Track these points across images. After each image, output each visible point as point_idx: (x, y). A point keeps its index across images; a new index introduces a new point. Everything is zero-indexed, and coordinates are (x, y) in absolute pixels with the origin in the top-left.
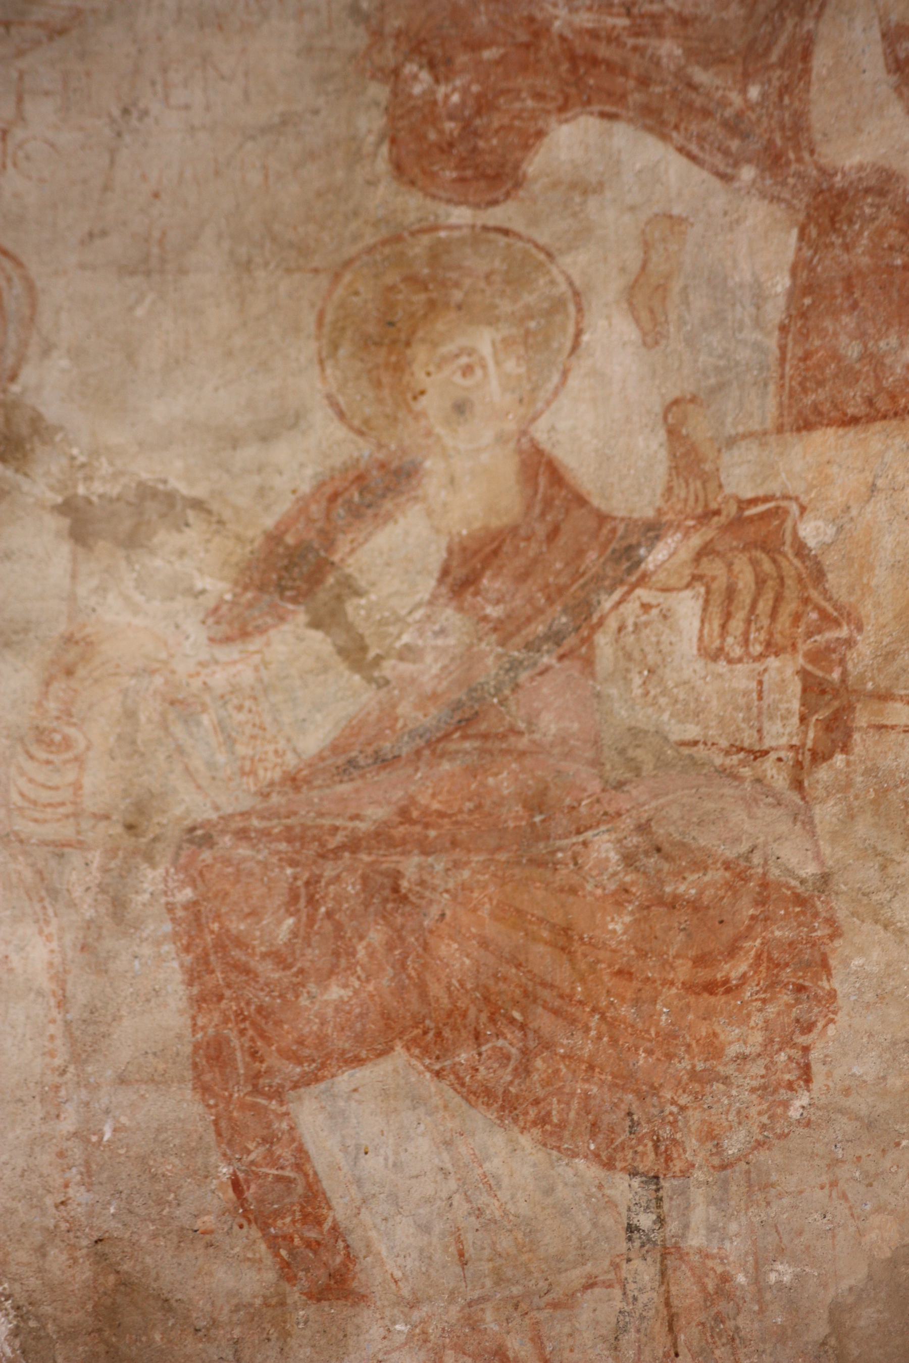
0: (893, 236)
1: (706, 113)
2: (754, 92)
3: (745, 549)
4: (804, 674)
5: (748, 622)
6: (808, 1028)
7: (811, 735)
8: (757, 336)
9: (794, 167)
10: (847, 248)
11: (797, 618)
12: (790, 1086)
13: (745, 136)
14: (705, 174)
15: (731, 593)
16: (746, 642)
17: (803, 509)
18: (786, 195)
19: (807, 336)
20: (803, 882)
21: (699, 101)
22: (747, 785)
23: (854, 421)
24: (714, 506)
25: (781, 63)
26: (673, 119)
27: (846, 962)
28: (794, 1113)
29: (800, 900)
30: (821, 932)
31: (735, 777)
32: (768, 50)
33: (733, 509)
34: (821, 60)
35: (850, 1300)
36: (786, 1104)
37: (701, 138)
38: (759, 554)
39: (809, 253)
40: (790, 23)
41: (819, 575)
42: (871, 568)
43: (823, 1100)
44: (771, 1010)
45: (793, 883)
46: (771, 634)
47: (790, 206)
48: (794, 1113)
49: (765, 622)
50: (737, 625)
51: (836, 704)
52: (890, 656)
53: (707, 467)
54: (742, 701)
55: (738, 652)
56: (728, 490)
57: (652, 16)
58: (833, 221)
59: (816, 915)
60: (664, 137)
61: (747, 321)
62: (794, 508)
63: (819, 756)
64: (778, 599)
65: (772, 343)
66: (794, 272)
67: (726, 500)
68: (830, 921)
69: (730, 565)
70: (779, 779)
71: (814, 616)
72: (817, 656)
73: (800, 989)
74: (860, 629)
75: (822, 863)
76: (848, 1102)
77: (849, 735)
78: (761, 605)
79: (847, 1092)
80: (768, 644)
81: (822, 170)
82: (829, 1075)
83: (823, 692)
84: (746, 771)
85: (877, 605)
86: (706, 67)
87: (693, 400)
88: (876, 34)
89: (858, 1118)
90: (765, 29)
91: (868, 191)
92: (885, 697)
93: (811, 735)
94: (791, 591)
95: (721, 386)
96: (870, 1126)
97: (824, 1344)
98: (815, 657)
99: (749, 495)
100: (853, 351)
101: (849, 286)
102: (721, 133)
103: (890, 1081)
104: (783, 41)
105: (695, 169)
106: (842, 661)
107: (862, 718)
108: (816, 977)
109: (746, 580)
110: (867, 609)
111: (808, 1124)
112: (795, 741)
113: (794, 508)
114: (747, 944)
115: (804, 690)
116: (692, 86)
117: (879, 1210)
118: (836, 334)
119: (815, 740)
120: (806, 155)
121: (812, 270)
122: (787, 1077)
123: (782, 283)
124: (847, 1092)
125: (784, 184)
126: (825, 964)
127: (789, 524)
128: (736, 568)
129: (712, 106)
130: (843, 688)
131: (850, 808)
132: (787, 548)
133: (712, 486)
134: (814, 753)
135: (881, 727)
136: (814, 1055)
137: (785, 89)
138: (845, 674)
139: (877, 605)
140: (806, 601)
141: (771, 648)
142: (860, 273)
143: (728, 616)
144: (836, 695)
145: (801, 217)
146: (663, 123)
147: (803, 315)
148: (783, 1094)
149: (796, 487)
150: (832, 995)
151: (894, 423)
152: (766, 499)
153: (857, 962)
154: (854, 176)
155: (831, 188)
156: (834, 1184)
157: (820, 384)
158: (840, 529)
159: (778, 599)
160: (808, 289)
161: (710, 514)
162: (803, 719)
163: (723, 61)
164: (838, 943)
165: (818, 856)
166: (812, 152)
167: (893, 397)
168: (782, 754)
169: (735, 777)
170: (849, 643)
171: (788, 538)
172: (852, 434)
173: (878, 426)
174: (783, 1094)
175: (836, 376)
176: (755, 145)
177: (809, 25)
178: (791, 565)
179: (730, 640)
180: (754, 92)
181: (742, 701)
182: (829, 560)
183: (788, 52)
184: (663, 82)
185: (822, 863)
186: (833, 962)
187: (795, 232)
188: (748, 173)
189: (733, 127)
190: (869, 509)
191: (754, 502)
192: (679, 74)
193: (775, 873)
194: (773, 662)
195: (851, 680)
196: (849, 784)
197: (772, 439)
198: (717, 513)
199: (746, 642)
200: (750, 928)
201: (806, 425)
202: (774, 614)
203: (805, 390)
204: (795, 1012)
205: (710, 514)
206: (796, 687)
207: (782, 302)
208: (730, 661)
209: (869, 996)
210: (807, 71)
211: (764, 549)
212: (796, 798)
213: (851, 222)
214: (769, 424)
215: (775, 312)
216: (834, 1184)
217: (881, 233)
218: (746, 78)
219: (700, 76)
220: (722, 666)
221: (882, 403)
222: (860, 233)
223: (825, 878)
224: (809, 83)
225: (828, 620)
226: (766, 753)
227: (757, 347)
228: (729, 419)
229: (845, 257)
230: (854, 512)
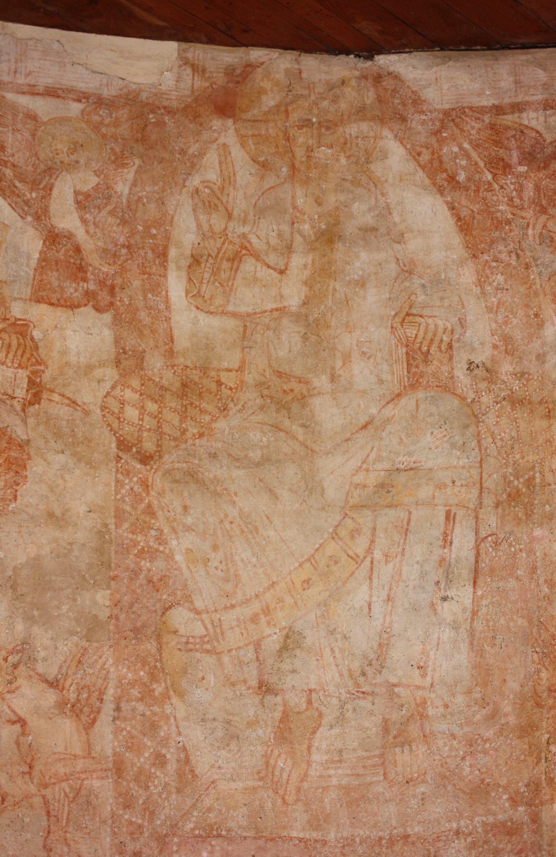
0: (71, 253)
1: (19, 196)
2: (34, 195)
3: (15, 333)
4: (29, 377)
5: (14, 356)
6: (18, 484)
7: (29, 396)
8: (26, 269)
9: (44, 221)
10: (57, 252)
11: (29, 359)
12: (10, 500)
13: (29, 207)
14: (16, 215)
15: (9, 346)
16: (13, 362)
17: (34, 326)
18: (40, 229)
19: (42, 274)
20: (22, 440)
21: (17, 192)
22: (8, 406)
23: (52, 304)
24: (8, 317)
25: (43, 189)
26: (8, 195)
27: (31, 468)
28: (10, 509)
29: (20, 446)
30: (25, 457)
31: (4, 402)
32: (39, 184)
33: (13, 320)
34: (55, 192)
35: (20, 566)
36: (8, 505)
37: (16, 203)
38: (19, 336)
39: (46, 249)
40: (47, 178)
41: (37, 348)
42: (52, 351)
43: (19, 507)
44: (8, 476)
45: (19, 440)
46: (20, 362)
47: (41, 233)
48: (10, 509)
49: (19, 358)
50: (11, 356)
51: (38, 389)
52: (55, 379)
53: (7, 305)
54: (9, 380)
55: (10, 364)
56: (12, 314)
57: (4, 161)
58: (54, 241)
59: (24, 451)
60: (5, 199)
61: (24, 264)
62: (32, 326)
63: (31, 404)
64: (24, 352)
65: (32, 273)
66: (40, 253)
67: (12, 316)
68: (28, 454)
69: (10, 337)
70: (18, 408)
71: (34, 360)
72: (34, 373)
73: (17, 472)
74: (47, 368)
75: (28, 437)
76: (27, 509)
77: (40, 399)
78: (18, 352)
79: (27, 506)
80: (19, 365)
81: (51, 225)
82: (22, 500)
83: (34, 384)
84: (8, 402)
85: (53, 362)
86: (20, 182)
87: (5, 282)
88: (72, 190)
89: (29, 515)
90: (39, 177)
91: (65, 236)
92: (52, 391)
93: (29, 396)
94: (28, 351)
95: (14, 281)
96: (32, 518)
97: (10, 577)
98: (33, 372)
99: (19, 317)
100: (56, 283)
101: (57, 263)
102: (22, 204)
103: (40, 506)
104: (44, 183)
105: (13, 212)
106: (40, 376)
107: (45, 395)
108: (22, 470)
109: (14, 343)
110: (50, 362)
111: (14, 513)
112: (24, 397)
113: (32, 326)
114: (3, 455)
115: (29, 382)
116: (16, 187)
117: (32, 543)
118: (51, 277)
119: (30, 398)
120: (48, 219)
121: (46, 255)
122: (10, 497)
123: (36, 256)
124: (27, 506)
125: (40, 226)
126: (25, 467)
127: (30, 330)
128: (12, 338)
129: (20, 194)
130: (40, 385)
131: (38, 422)
132: (28, 337)
133: (8, 311)
134: (29, 402)
135: (50, 400)
136: (18, 493)
137: (43, 197)
138: (41, 381)
139: (53, 362)
140: (32, 355)
141: (20, 366)
142: (60, 261)
143: (8, 353)
144: (38, 386)
145: (44, 237)
146: (5, 194)
147: (42, 268)
148: (8, 502)
149: (33, 319)
150: (26, 477)
151: (65, 309)
152: (24, 320)
153: (35, 469)
154: (61, 231)
155: (54, 232)
156: (20, 532)
157: (44, 290)
158: (45, 336)
159: (24, 352)
160: (44, 260)
161: (5, 319)
162: (27, 391)
163: (25, 182)
164: (29, 462)
165: (27, 434)
166: (50, 219)
167: (66, 301)
168: (20, 400)
169: (4, 402)
170: (43, 371)
171: (29, 334)
172: (51, 308)
173: (60, 308)
174: (8, 502)
175: (49, 289)
176: (32, 211)
177: (52, 181)
178: (29, 343)
179: (8, 360)
180: (34, 195)
181: (9, 380)
182: (41, 344)
183: (45, 187)
184: (6, 182)
185: (28, 437)
186: (28, 467)
187: (42, 242)
188: (29, 219)
189: (26, 203)
190: (54, 332)
191: (20, 320)
192: (11, 181)
193: (14, 435)
194: (20, 371)
195: (43, 383)
196: (39, 415)
197: (28, 302)
198: (8, 319)
199: (13, 362)
200: (4, 450)
201: (38, 301)
202: (22, 356)
203: (40, 291)
204: (14, 479)
205: (5, 319)
206: (26, 380)
207: (36, 261)
208: (7, 367)
209: (37, 480)
210: (50, 194)
211: (21, 335)
212: (23, 414)
213: (59, 244)
214: (27, 297)
215: (34, 263)
216: (20, 532)
217: (67, 251)
218: (32, 190)
219: (18, 184)
220: (4, 367)
221: (62, 302)
222: (61, 249)
223: (29, 441)
224: (50, 198)
225: (38, 363)
226: (15, 398)
227: (27, 273)
228: (16, 292)
229: (56, 254)
230: (49, 332)
